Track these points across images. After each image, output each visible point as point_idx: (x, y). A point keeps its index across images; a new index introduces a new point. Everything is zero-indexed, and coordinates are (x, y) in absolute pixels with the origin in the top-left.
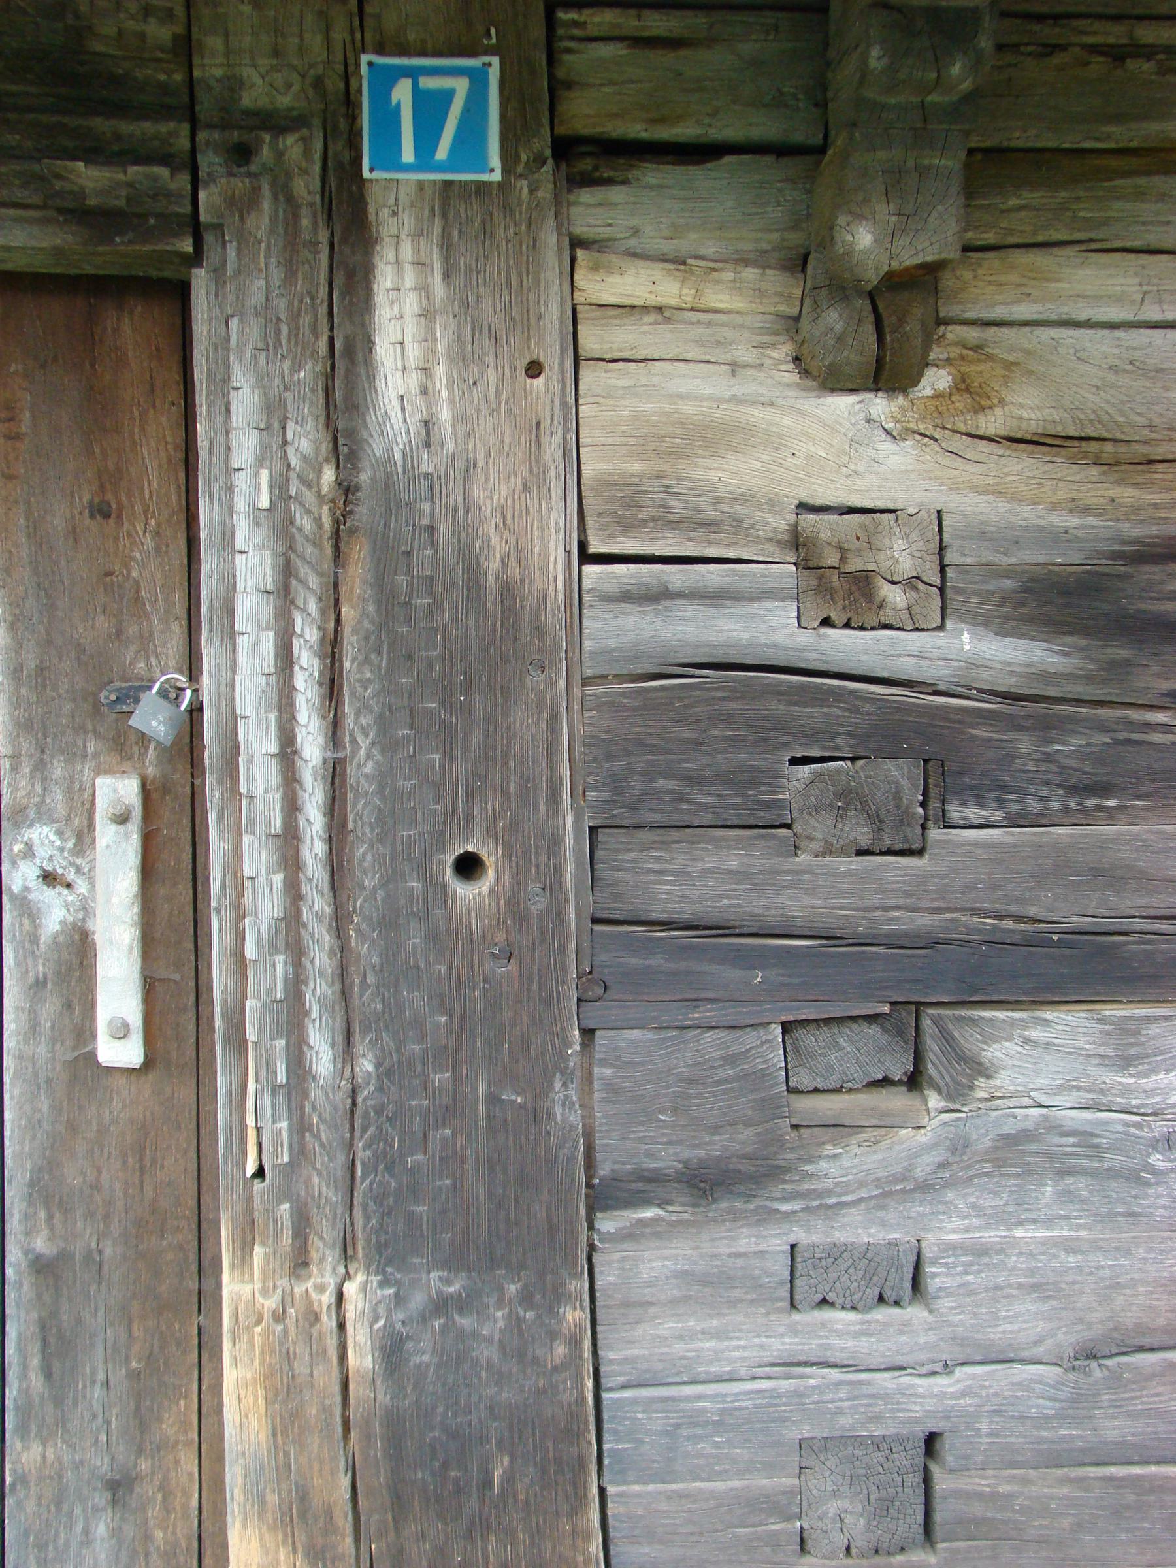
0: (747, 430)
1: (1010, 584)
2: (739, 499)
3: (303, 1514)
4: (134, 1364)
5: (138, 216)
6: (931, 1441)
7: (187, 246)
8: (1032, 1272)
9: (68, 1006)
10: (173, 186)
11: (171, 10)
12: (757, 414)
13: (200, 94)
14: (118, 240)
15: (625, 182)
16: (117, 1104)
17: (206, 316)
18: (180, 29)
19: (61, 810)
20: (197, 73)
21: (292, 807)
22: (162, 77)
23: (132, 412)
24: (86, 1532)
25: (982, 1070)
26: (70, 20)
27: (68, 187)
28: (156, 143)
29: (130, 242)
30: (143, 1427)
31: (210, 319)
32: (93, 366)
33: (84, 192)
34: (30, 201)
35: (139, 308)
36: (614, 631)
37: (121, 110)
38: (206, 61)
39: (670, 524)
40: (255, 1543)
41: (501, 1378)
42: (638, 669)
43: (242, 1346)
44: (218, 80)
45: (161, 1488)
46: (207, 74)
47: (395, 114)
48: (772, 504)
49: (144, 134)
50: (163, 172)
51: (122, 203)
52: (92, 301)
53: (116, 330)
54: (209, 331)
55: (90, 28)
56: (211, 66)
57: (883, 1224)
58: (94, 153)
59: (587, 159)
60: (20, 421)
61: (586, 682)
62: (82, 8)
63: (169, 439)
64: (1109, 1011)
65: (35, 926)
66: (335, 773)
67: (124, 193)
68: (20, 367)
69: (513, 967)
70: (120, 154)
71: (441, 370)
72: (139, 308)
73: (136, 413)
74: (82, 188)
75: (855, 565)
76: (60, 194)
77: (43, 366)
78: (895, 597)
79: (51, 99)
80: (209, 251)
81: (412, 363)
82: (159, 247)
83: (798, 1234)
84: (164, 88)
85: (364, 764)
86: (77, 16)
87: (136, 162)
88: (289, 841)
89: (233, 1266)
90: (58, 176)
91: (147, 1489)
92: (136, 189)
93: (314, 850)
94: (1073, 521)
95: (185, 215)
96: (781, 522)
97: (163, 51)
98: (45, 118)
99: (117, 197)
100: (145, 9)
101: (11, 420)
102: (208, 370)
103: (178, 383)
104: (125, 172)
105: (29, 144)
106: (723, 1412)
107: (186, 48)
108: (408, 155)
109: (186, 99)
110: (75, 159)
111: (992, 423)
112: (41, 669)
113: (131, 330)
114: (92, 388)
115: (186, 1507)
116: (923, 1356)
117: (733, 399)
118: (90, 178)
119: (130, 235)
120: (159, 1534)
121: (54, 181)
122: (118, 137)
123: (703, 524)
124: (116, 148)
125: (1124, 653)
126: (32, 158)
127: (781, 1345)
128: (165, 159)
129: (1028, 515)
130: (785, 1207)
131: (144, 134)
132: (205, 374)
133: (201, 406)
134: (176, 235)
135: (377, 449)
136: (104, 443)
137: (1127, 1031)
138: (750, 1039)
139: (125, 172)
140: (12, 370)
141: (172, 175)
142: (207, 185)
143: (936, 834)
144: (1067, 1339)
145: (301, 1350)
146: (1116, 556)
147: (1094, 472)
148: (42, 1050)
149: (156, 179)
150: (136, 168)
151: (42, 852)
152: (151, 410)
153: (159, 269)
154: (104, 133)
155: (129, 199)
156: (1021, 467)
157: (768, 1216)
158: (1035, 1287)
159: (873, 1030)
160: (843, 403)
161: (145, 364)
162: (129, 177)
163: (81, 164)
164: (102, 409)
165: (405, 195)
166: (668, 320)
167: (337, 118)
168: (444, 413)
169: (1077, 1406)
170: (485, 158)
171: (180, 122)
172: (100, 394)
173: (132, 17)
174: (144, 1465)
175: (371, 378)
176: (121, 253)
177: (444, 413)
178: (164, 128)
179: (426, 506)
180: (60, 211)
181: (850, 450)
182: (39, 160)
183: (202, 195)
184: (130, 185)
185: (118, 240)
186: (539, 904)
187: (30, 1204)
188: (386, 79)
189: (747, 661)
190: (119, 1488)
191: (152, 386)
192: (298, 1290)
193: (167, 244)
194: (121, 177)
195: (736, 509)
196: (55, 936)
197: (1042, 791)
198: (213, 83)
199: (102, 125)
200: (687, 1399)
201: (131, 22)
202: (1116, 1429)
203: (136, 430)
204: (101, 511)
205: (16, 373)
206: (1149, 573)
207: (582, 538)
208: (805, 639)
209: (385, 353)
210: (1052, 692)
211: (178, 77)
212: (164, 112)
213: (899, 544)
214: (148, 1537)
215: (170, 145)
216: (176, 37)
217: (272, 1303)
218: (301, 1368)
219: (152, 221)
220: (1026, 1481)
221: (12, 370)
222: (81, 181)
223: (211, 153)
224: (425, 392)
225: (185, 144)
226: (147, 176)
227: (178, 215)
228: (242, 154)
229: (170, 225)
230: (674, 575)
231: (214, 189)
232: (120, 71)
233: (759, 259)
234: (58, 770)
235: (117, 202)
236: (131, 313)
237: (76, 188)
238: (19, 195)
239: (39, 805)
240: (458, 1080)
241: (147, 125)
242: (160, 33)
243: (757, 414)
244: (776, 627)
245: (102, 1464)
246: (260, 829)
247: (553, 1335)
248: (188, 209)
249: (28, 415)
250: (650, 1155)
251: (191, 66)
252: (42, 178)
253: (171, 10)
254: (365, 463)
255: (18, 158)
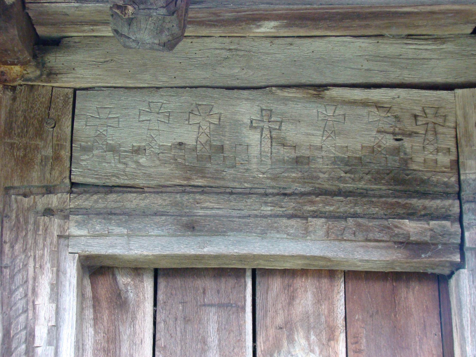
1: (87, 282)
5: (433, 244)
7: (457, 258)
10: (452, 230)
11: (449, 149)
13: (464, 186)
14: (423, 256)
17: (468, 293)
18: (454, 158)
20: (462, 177)
22: (446, 180)
23: (415, 339)
26: (402, 155)
27: (401, 232)
28: (443, 210)
29: (430, 257)
31: (470, 294)
32: (395, 316)
33: (409, 234)
34: (383, 239)
35: (417, 287)
37: (424, 195)
38: (467, 172)
44: (474, 180)
46: (468, 178)
49: (437, 206)
50: (447, 223)
51: (427, 239)
52: (394, 284)
53: (406, 298)
54: (470, 300)
55: (411, 158)
56: (469, 174)
58: (412, 214)
60: (361, 343)
62: (408, 150)
63: (434, 352)
67: (429, 233)
68: (360, 317)
70: (424, 215)
72: (417, 287)
73: (417, 339)
74: (408, 231)
76: (397, 235)
77: (371, 316)
79: (391, 191)
80: (468, 260)
82: (443, 259)
84: (446, 184)
86: (405, 154)
87: (432, 219)
90: (396, 227)
92: (434, 232)
95: (456, 244)
97: (446, 168)
98: (390, 200)
99: (426, 236)
100: (437, 149)
101: (356, 343)
102: (471, 319)
103: (437, 324)
104: (428, 224)
105: (382, 212)
107: (457, 165)
109: (457, 189)
110: (403, 218)
113: (415, 298)
114: (395, 327)
118: (411, 227)
119: (429, 254)
121: (395, 229)
122: (425, 208)
124: (423, 213)
126: (382, 218)
128: (446, 217)
131: (437, 206)
132: (469, 322)
133: (468, 337)
134: (452, 253)
136: (402, 354)
139: (428, 224)
140: (356, 318)
141: (452, 225)
142: (468, 230)
149: (444, 227)
150: (434, 222)
152: (425, 338)
153: (433, 269)
154: (418, 206)
155: (431, 237)
161: (421, 315)
162: (431, 227)
163: (407, 221)
164: (401, 337)
171: (454, 200)
172: (399, 330)
173: (431, 153)
176: (424, 262)
178: (448, 202)
180: (395, 243)
182: (387, 219)
183: (467, 234)
184: (431, 230)
185: (423, 256)
189: (152, 342)
191: (425, 326)
193: (447, 258)
194: (427, 226)
198: (471, 182)
199: (416, 202)
201: (431, 155)
203: (418, 348)
205: (358, 320)
207: (155, 308)
211: (453, 179)
212: (445, 195)
215: (450, 211)
216: (451, 161)
219: (440, 247)
221: (356, 318)
222: (407, 229)
223: (470, 214)
225: (457, 210)
226: (440, 226)
227: (454, 243)
229: (447, 247)
231: (472, 231)
232: (426, 178)
235: (426, 239)
236: (413, 290)
237: (405, 232)
238: (378, 236)
241: (438, 201)
242: (445, 160)
248: (459, 241)
249: (364, 340)
251: (459, 175)
252: (389, 228)
253: (449, 149)
255: (374, 218)
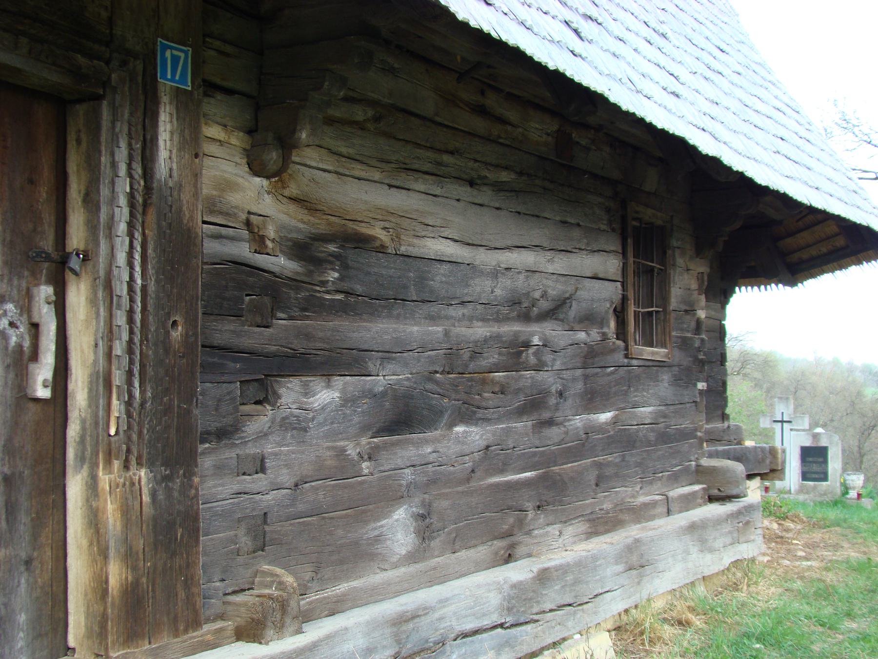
0: (237, 184)
2: (236, 207)
3: (130, 555)
4: (33, 516)
6: (265, 514)
8: (285, 461)
9: (17, 375)
12: (240, 180)
15: (213, 97)
16: (30, 414)
19: (16, 297)
20: (114, 32)
21: (132, 300)
24: (19, 582)
25: (279, 397)
30: (35, 540)
36: (211, 247)
39: (221, 213)
40: (117, 566)
41: (179, 502)
42: (215, 261)
43: (113, 496)
45: (40, 562)
47: (166, 60)
48: (243, 210)
57: (256, 447)
59: (210, 88)
61: (206, 263)
64: (304, 379)
65: (7, 343)
66: (144, 288)
69: (185, 360)
71: (174, 151)
75: (261, 233)
78: (270, 244)
81: (168, 148)
83: (238, 451)
85: (152, 287)
88: (131, 312)
89: (103, 469)
91: (36, 563)
93: (138, 317)
94: (301, 226)
96: (244, 216)
106: (223, 511)
107: (111, 22)
108: (169, 77)
111: (287, 192)
112: (11, 241)
115: (47, 569)
116: (264, 489)
117: (236, 175)
120: (39, 580)
123: (227, 214)
125: (312, 268)
127: (236, 488)
129: (294, 223)
130: (237, 442)
135: (158, 176)
137: (306, 385)
138: (232, 386)
143: (274, 321)
144: (293, 480)
145: (130, 497)
146: (310, 238)
147: (306, 211)
148: (9, 393)
151: (10, 314)
156: (292, 208)
157: (234, 445)
158: (286, 465)
159: (256, 384)
160: (258, 180)
165: (168, 88)
166: (222, 145)
167: (150, 59)
168: (175, 166)
169: (294, 500)
170: (187, 82)
174: (35, 554)
175: (157, 151)
177: (175, 166)
179: (170, 198)
181: (252, 194)
186: (192, 339)
187: (3, 454)
188: (165, 48)
190: (28, 563)
192: (128, 475)
195: (236, 211)
196: (14, 347)
197: (295, 309)
200: (216, 507)
202: (301, 507)
204: (31, 182)
206: (317, 244)
208: (250, 255)
209: (161, 143)
210: (298, 278)
213: (271, 228)
214: (36, 582)
217: (122, 480)
218: (130, 503)
220: (283, 526)
224: (170, 158)
228: (124, 63)
230: (224, 231)
233: (240, 129)
234: (15, 282)
239: (10, 295)
240: (170, 400)
243: (240, 180)
244: (243, 251)
245: (23, 555)
246: (124, 308)
247: (191, 487)
250: (210, 425)
254: (155, 181)
